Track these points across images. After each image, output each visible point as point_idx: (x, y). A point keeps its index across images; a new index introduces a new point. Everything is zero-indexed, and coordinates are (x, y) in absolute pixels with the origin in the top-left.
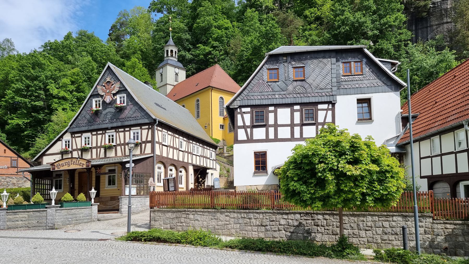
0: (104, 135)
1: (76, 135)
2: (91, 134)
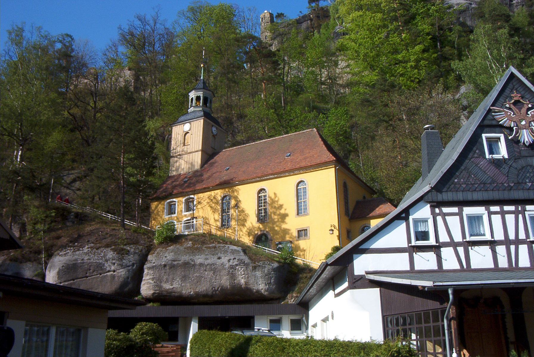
0: (520, 216)
1: (446, 210)
2: (488, 210)
